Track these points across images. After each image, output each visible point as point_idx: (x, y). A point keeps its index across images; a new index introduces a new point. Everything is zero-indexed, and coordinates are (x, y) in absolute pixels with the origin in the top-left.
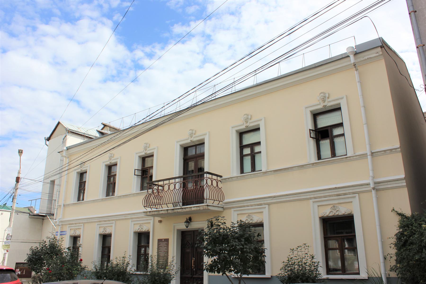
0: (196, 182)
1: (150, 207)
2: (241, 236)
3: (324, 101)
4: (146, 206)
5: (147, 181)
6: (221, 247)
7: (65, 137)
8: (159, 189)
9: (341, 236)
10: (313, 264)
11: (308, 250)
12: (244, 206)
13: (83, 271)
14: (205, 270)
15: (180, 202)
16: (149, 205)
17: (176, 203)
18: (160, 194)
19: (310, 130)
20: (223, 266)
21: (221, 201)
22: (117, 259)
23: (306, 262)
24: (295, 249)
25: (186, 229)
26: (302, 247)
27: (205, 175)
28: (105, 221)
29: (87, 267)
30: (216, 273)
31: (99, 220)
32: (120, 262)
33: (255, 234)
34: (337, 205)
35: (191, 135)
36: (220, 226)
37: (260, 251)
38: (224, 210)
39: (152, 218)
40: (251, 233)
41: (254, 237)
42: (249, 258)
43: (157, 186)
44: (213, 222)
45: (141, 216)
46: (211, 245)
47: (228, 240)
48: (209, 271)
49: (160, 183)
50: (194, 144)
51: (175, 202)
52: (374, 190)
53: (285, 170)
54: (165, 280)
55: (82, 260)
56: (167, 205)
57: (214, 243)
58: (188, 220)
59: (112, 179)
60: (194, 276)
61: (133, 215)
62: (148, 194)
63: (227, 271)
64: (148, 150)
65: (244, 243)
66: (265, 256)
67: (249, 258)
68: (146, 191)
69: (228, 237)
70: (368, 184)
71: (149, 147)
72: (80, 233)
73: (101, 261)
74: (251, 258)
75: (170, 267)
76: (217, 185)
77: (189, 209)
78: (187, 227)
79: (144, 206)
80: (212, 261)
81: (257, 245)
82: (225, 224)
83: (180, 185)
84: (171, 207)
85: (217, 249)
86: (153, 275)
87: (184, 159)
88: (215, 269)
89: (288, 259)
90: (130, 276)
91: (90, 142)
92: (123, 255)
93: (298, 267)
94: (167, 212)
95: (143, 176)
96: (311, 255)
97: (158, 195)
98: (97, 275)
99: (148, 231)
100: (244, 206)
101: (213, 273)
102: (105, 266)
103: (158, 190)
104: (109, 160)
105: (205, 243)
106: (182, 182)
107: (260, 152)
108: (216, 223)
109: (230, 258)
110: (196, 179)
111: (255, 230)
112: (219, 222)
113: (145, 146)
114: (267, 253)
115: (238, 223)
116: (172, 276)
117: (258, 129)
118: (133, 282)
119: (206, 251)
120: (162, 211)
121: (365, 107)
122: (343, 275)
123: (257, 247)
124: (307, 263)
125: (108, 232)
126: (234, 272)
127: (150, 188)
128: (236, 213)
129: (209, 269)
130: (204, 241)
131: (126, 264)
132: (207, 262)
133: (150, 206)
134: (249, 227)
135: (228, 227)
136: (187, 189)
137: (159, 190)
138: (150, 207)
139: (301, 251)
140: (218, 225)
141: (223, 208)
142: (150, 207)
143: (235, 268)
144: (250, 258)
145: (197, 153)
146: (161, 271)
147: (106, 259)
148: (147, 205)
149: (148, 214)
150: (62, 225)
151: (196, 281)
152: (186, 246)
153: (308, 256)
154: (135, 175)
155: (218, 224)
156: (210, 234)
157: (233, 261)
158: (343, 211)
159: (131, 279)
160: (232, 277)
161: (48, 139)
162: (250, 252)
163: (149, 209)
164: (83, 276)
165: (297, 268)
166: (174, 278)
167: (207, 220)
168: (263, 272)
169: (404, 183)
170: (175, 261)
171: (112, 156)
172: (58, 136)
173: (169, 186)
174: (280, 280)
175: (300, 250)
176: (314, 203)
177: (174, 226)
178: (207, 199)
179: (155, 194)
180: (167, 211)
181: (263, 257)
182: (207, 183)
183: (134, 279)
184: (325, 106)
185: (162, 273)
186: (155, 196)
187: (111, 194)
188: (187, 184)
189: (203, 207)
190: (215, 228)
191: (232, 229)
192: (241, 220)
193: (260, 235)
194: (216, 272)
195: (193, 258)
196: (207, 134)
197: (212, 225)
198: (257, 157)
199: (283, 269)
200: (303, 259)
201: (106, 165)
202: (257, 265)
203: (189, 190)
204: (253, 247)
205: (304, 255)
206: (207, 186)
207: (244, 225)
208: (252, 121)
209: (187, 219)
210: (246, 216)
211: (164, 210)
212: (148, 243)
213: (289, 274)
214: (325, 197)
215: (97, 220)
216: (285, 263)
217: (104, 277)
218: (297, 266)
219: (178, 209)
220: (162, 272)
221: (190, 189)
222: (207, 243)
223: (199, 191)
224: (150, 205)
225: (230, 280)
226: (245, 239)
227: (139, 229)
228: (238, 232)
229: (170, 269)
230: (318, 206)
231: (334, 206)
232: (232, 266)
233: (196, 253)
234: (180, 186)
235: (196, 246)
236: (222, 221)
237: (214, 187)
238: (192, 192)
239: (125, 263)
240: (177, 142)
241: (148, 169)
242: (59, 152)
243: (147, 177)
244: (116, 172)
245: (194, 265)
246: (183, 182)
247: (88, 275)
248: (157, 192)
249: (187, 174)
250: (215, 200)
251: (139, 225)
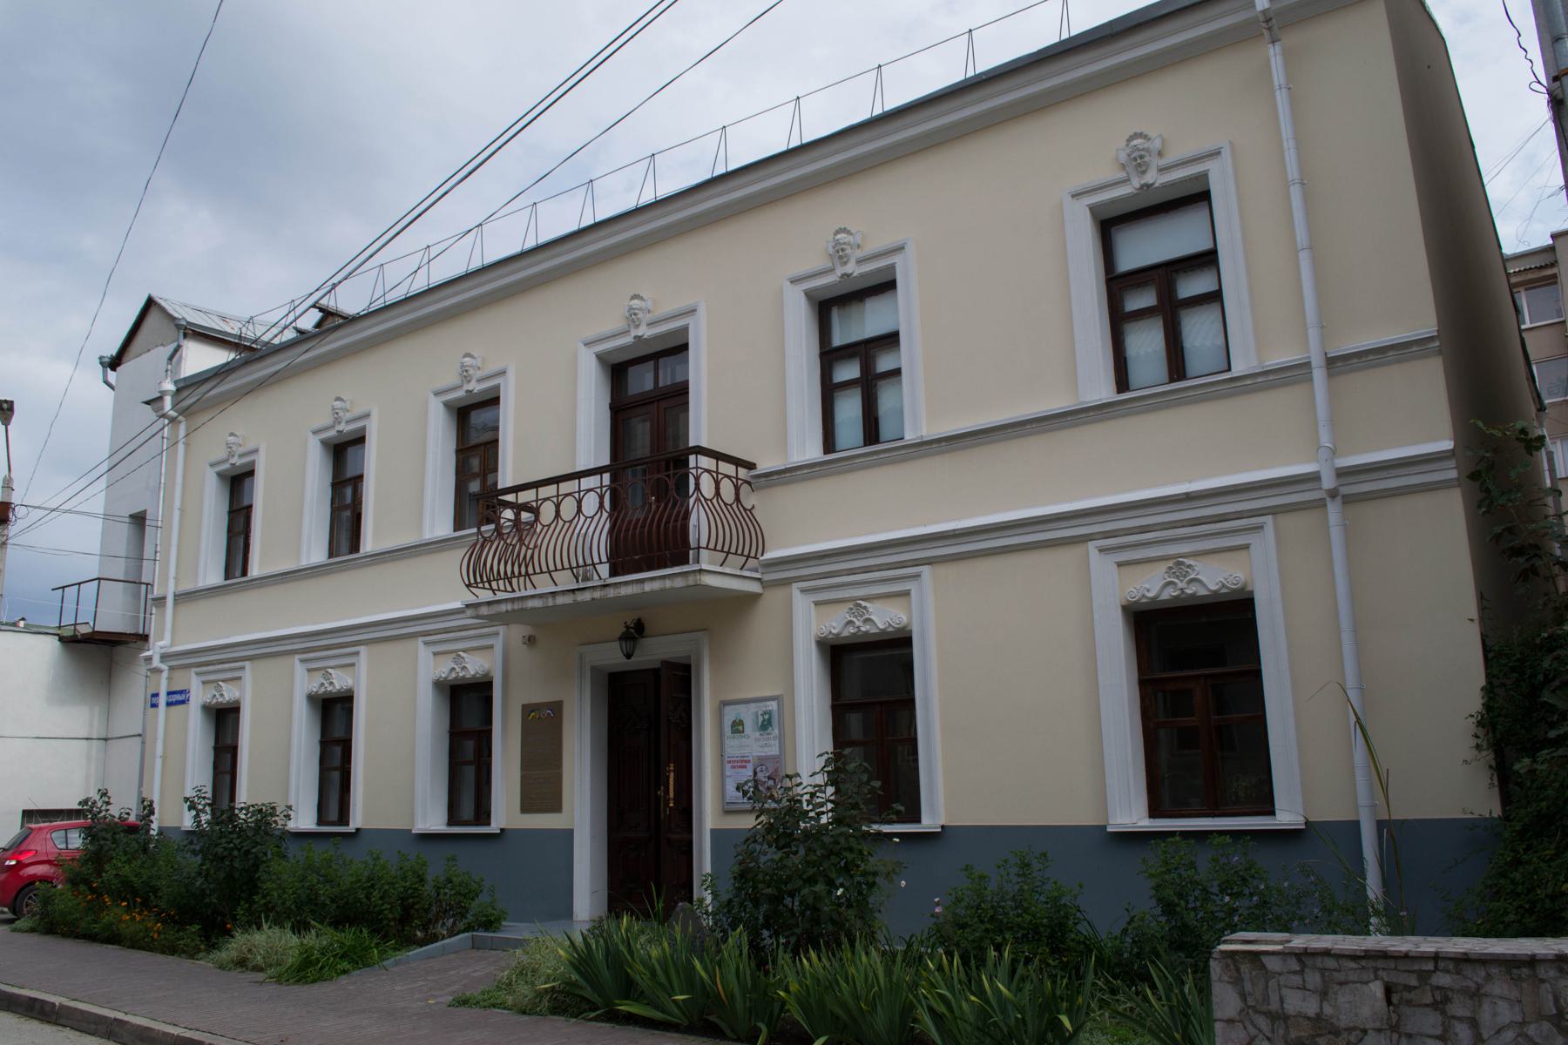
1: (491, 588)
3: (1142, 168)
4: (472, 581)
7: (176, 350)
9: (1206, 676)
15: (601, 563)
21: (753, 554)
27: (692, 458)
49: (526, 497)
51: (581, 562)
56: (551, 575)
58: (632, 631)
59: (349, 492)
70: (1314, 478)
76: (737, 499)
78: (628, 656)
79: (467, 583)
87: (611, 408)
110: (659, 476)
117: (885, 286)
121: (1304, 184)
122: (1210, 819)
138: (490, 585)
141: (762, 583)
142: (490, 585)
149: (484, 611)
158: (883, 617)
161: (114, 363)
163: (485, 595)
169: (1450, 471)
172: (149, 351)
173: (558, 506)
182: (699, 490)
209: (627, 627)
211: (541, 596)
224: (481, 577)
234: (598, 505)
237: (726, 504)
242: (147, 403)
250: (728, 553)
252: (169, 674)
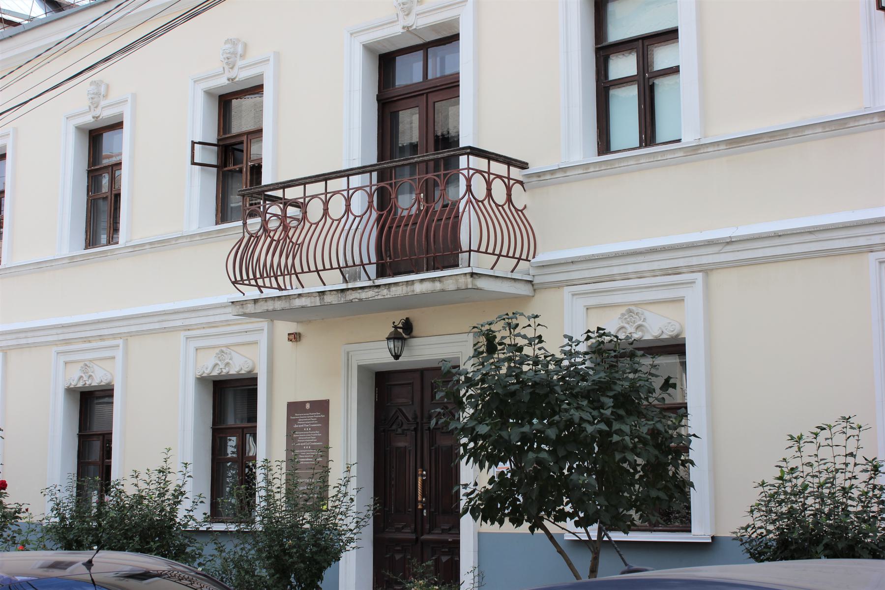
0: (428, 190)
2: (603, 387)
4: (239, 278)
5: (241, 184)
6: (526, 429)
8: (290, 217)
10: (877, 492)
11: (858, 440)
12: (611, 279)
13: (12, 524)
14: (465, 512)
15: (370, 263)
16: (251, 276)
17: (354, 265)
18: (290, 235)
19: (193, 143)
20: (534, 498)
21: (524, 257)
22: (137, 477)
23: (847, 484)
24: (808, 436)
25: (393, 362)
26: (833, 430)
27: (463, 160)
28: (87, 340)
29: (27, 510)
30: (508, 527)
31: (61, 337)
32: (147, 485)
33: (653, 379)
36: (520, 349)
37: (673, 444)
38: (535, 290)
39: (264, 324)
40: (637, 376)
41: (651, 391)
42: (632, 471)
43: (281, 206)
44: (496, 334)
45: (223, 318)
46: (487, 422)
47: (553, 402)
48: (480, 517)
49: (292, 193)
50: (419, 42)
51: (350, 263)
53: (771, 137)
54: (321, 550)
55: (6, 485)
57: (501, 414)
58: (400, 330)
59: (105, 181)
60: (426, 537)
61: (193, 315)
62: (246, 234)
63: (549, 516)
64: (241, 68)
65: (612, 413)
66: (692, 463)
67: (632, 471)
68: (240, 223)
69: (553, 391)
71: (242, 56)
73: (79, 487)
74: (639, 468)
75: (337, 503)
76: (509, 199)
77: (404, 288)
78: (397, 357)
79: (233, 280)
80: (491, 481)
81: (660, 421)
82: (541, 341)
83: (367, 198)
84: (334, 281)
85: (513, 434)
86: (274, 532)
87: (379, 99)
88: (503, 508)
89: (782, 471)
90: (186, 537)
91: (11, 37)
92: (160, 464)
93: (819, 503)
94: (322, 299)
95: (226, 166)
96: (870, 459)
97: (285, 240)
98: (65, 538)
99: (250, 372)
100: (611, 279)
101: (496, 523)
102: (95, 505)
103: (283, 218)
104: (90, 107)
105: (465, 414)
106: (374, 188)
107: (675, 70)
108: (508, 338)
109: (562, 469)
110: (429, 176)
111: (653, 366)
112: (519, 335)
113: (229, 53)
114: (697, 452)
115: (588, 338)
116: (344, 534)
118: (201, 560)
119: (470, 441)
120: (303, 299)
123: (662, 429)
124: (852, 491)
125: (97, 379)
126: (576, 522)
127: (255, 210)
128: (581, 303)
129: (483, 510)
130: (461, 406)
131: (173, 495)
132: (473, 483)
133: (255, 279)
134: (632, 355)
135: (553, 355)
136: (396, 213)
137: (288, 220)
138: (256, 282)
139: (829, 445)
140: (516, 345)
141: (533, 285)
142: (256, 282)
143: (578, 504)
144: (635, 469)
145: (430, 77)
146: (304, 519)
147: (98, 478)
148: (245, 277)
149: (250, 308)
151: (433, 556)
152: (394, 427)
153: (855, 465)
154: (193, 163)
155: (513, 343)
156: (483, 381)
157: (572, 477)
159: (193, 551)
160: (566, 538)
162: (635, 447)
163: (252, 293)
164: (11, 542)
165: (811, 506)
166: (353, 545)
167: (474, 327)
168: (682, 522)
170: (353, 484)
171: (103, 90)
173: (326, 203)
174: (748, 551)
175: (826, 439)
177: (348, 353)
178: (470, 251)
179: (272, 234)
180: (320, 296)
181: (685, 466)
183: (202, 550)
185: (307, 526)
186: (274, 243)
187: (104, 238)
188: (393, 196)
189: (457, 281)
190: (502, 356)
191: (566, 363)
192: (599, 329)
193: (674, 386)
194: (507, 520)
195: (420, 473)
197: (492, 348)
198: (663, 88)
199: (759, 510)
200: (838, 475)
201: (79, 129)
202: (662, 495)
203: (402, 218)
204: (644, 430)
205: (842, 459)
206: (471, 202)
207: (611, 346)
209: (396, 327)
210: (80, 369)
211: (309, 295)
212: (252, 417)
213: (783, 529)
215: (55, 338)
216: (766, 489)
217: (91, 543)
218: (813, 501)
219: (360, 291)
220: (308, 522)
221: (405, 213)
222: (473, 414)
223: (440, 220)
225: (560, 551)
226: (615, 397)
227: (216, 365)
228: (591, 372)
229: (337, 510)
231: (629, 309)
232: (565, 500)
233: (430, 450)
235: (433, 422)
236: (530, 332)
237: (497, 205)
238: (415, 224)
239: (167, 491)
241: (244, 138)
243: (241, 171)
244: (121, 154)
245: (423, 497)
246: (377, 189)
247: (33, 537)
248: (281, 228)
249: (392, 157)
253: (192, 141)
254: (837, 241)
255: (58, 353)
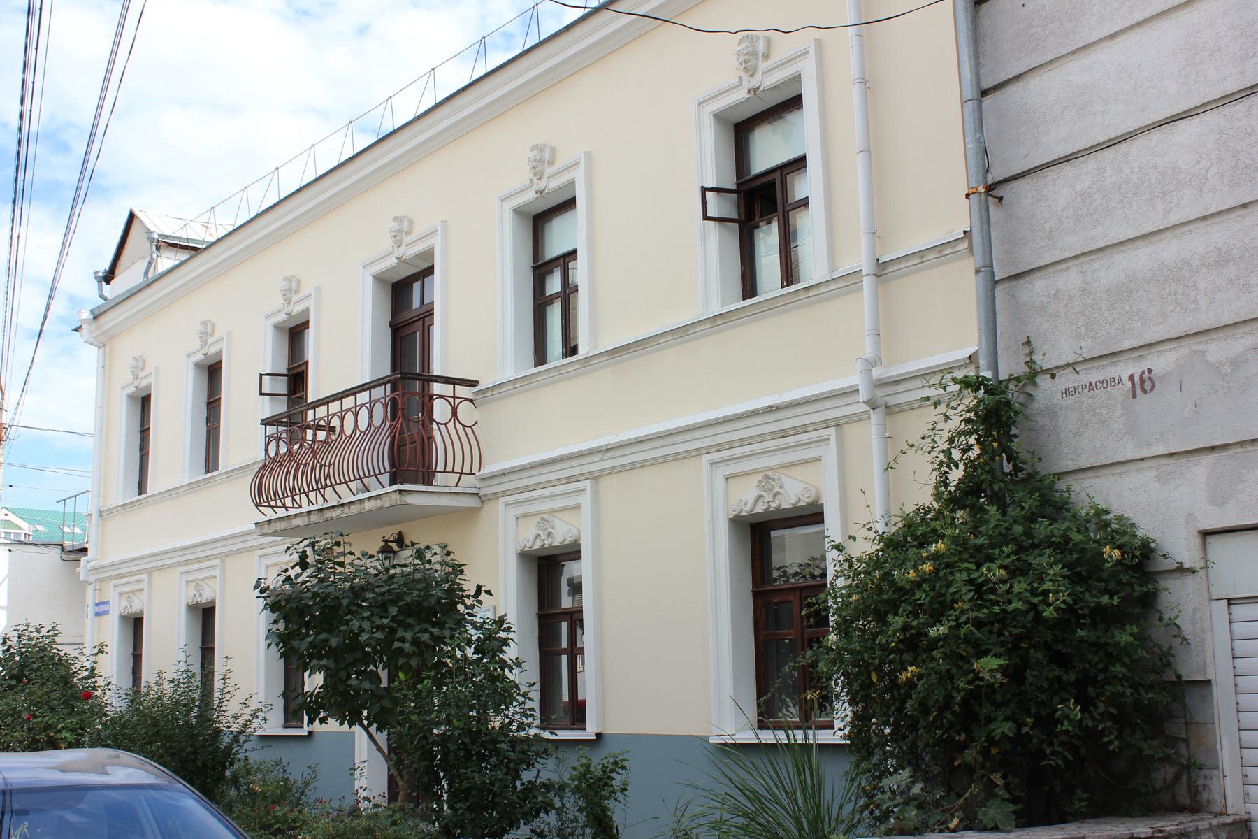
12: (531, 488)
19: (704, 190)
34: (780, 471)
35: (537, 169)
38: (482, 502)
52: (876, 410)
70: (852, 391)
72: (580, 533)
100: (531, 488)
106: (388, 399)
120: (298, 519)
125: (560, 535)
141: (480, 497)
150: (100, 580)
154: (706, 218)
176: (714, 466)
184: (756, 90)
196: (436, 231)
208: (559, 165)
209: (386, 541)
210: (535, 524)
214: (746, 442)
230: (727, 478)
240: (364, 267)
246: (390, 400)
251: (760, 477)
252: (884, 426)
253: (702, 187)
254: (681, 445)
255: (712, 464)
